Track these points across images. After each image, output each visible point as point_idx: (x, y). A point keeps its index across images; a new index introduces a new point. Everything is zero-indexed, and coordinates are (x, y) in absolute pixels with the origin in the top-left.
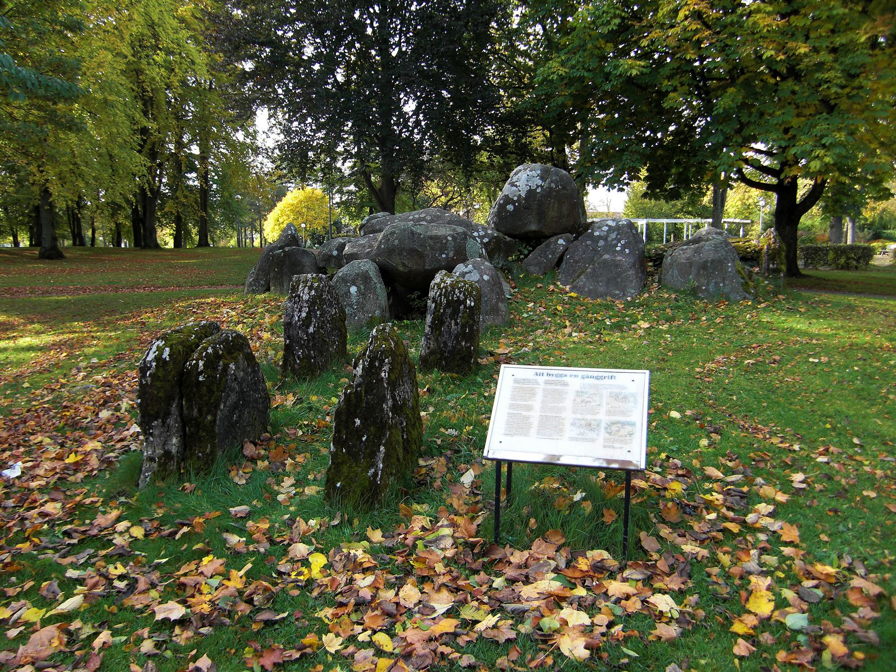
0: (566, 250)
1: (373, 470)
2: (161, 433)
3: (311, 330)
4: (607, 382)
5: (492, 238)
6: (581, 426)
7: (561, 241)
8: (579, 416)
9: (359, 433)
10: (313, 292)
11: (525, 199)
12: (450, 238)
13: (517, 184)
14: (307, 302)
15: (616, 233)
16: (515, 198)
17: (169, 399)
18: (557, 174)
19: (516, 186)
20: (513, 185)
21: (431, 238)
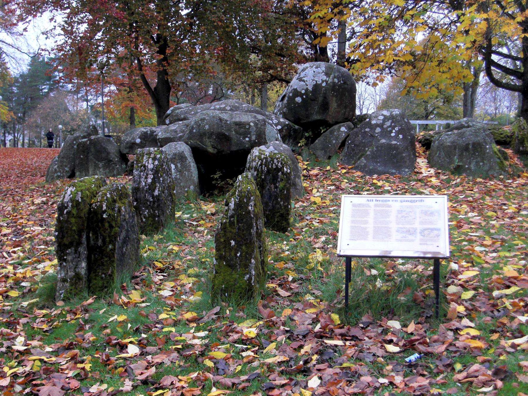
0: (348, 136)
1: (248, 276)
2: (74, 258)
3: (156, 193)
4: (418, 204)
5: (284, 125)
6: (403, 232)
7: (343, 129)
8: (401, 226)
10: (156, 162)
11: (311, 92)
12: (252, 124)
13: (305, 79)
14: (152, 170)
15: (390, 121)
16: (303, 92)
17: (80, 233)
18: (339, 71)
19: (304, 81)
20: (300, 80)
21: (237, 124)
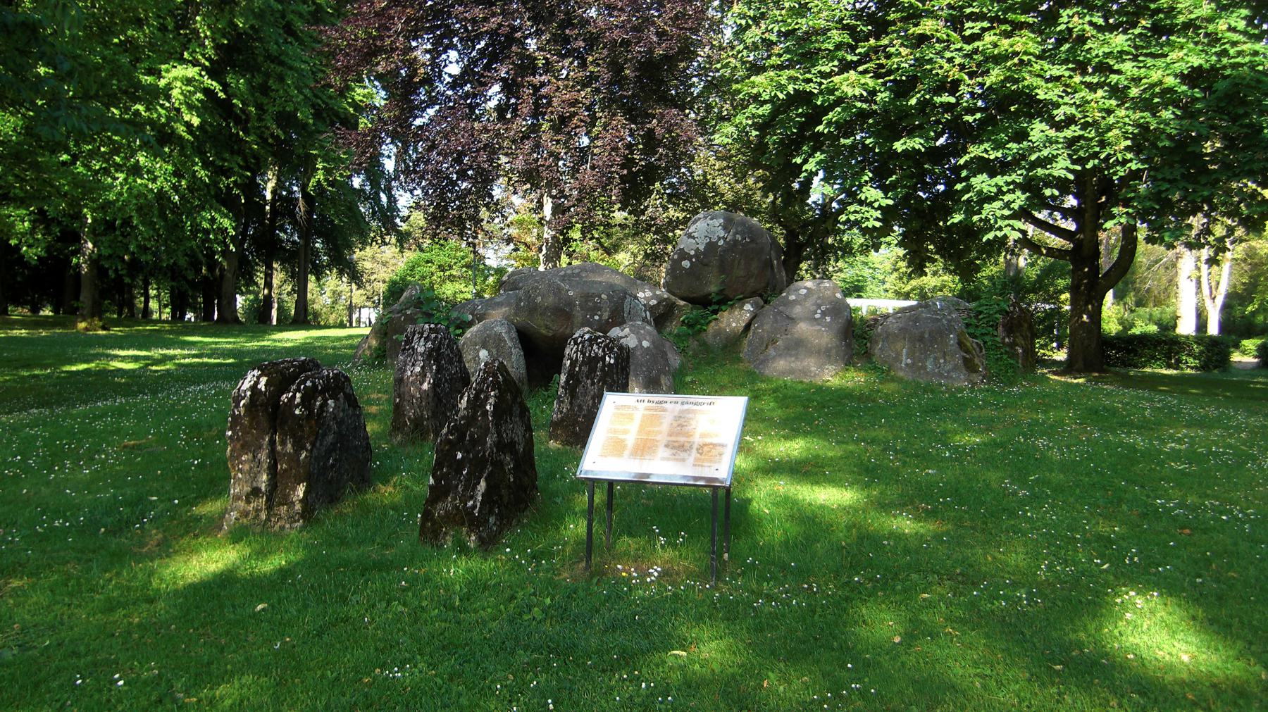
6: (673, 448)
9: (460, 465)
10: (429, 345)
13: (695, 235)
14: (422, 355)
16: (692, 253)
